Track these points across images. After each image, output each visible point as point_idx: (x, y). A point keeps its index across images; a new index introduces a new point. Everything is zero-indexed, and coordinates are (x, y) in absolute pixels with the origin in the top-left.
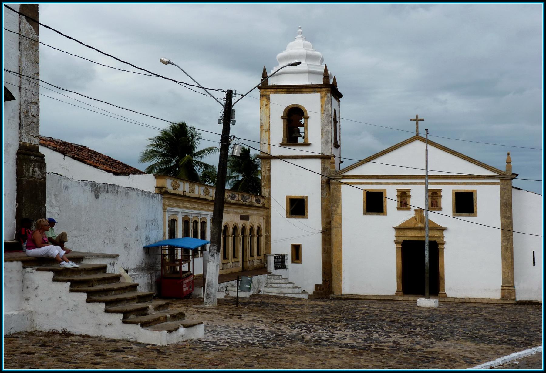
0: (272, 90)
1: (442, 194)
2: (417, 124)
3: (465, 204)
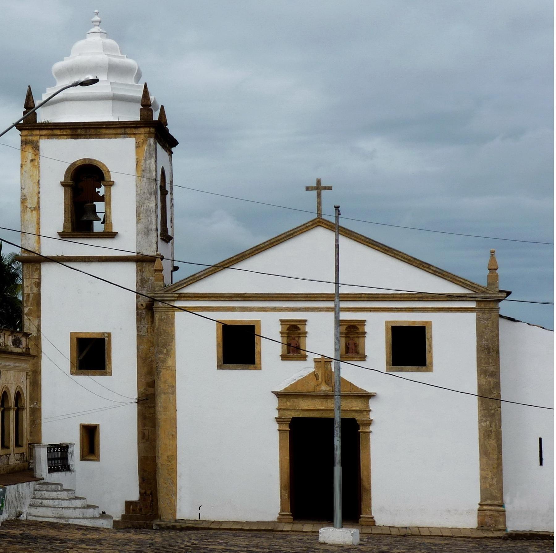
0: (44, 132)
2: (319, 195)
3: (409, 348)
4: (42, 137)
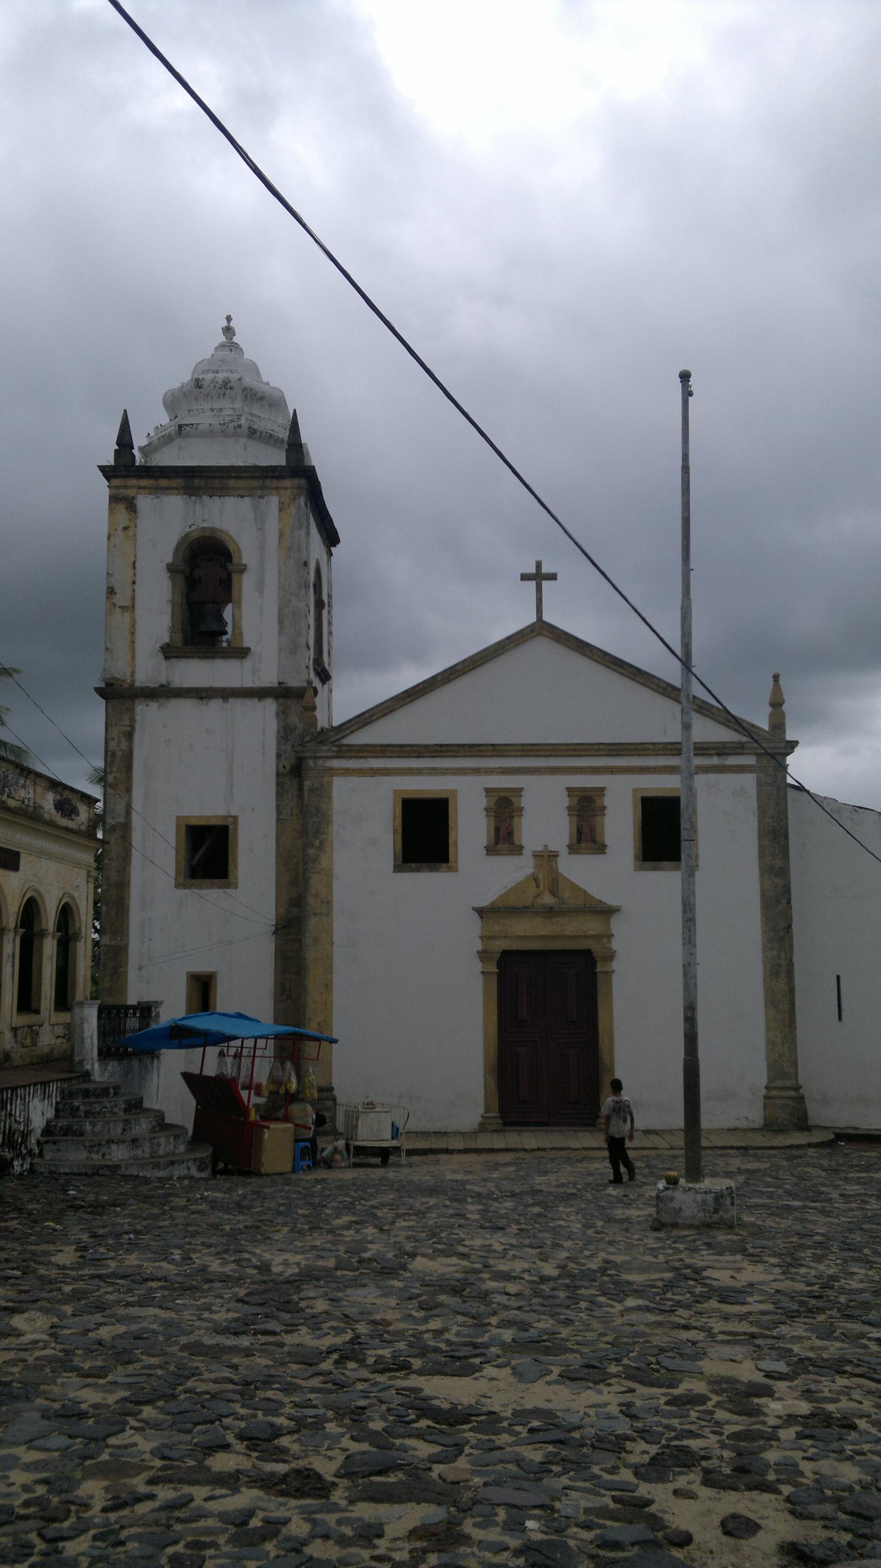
0: (145, 482)
1: (524, 802)
2: (539, 589)
3: (663, 833)
4: (141, 491)
